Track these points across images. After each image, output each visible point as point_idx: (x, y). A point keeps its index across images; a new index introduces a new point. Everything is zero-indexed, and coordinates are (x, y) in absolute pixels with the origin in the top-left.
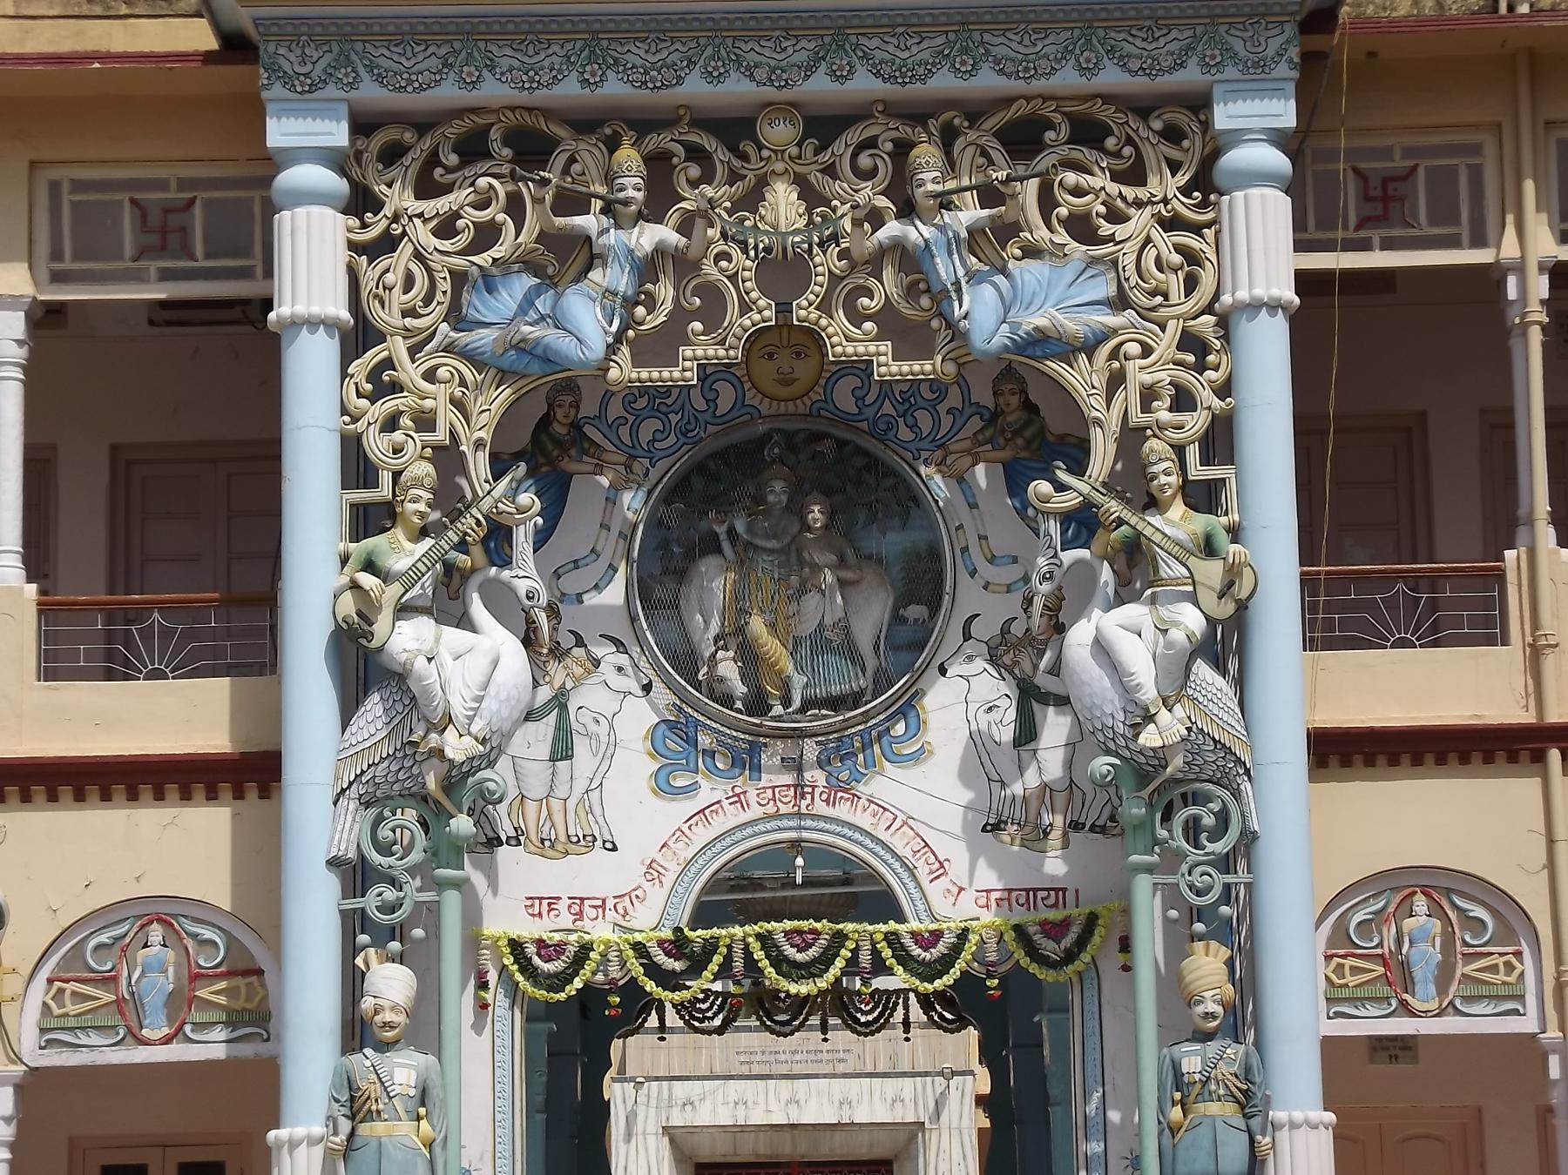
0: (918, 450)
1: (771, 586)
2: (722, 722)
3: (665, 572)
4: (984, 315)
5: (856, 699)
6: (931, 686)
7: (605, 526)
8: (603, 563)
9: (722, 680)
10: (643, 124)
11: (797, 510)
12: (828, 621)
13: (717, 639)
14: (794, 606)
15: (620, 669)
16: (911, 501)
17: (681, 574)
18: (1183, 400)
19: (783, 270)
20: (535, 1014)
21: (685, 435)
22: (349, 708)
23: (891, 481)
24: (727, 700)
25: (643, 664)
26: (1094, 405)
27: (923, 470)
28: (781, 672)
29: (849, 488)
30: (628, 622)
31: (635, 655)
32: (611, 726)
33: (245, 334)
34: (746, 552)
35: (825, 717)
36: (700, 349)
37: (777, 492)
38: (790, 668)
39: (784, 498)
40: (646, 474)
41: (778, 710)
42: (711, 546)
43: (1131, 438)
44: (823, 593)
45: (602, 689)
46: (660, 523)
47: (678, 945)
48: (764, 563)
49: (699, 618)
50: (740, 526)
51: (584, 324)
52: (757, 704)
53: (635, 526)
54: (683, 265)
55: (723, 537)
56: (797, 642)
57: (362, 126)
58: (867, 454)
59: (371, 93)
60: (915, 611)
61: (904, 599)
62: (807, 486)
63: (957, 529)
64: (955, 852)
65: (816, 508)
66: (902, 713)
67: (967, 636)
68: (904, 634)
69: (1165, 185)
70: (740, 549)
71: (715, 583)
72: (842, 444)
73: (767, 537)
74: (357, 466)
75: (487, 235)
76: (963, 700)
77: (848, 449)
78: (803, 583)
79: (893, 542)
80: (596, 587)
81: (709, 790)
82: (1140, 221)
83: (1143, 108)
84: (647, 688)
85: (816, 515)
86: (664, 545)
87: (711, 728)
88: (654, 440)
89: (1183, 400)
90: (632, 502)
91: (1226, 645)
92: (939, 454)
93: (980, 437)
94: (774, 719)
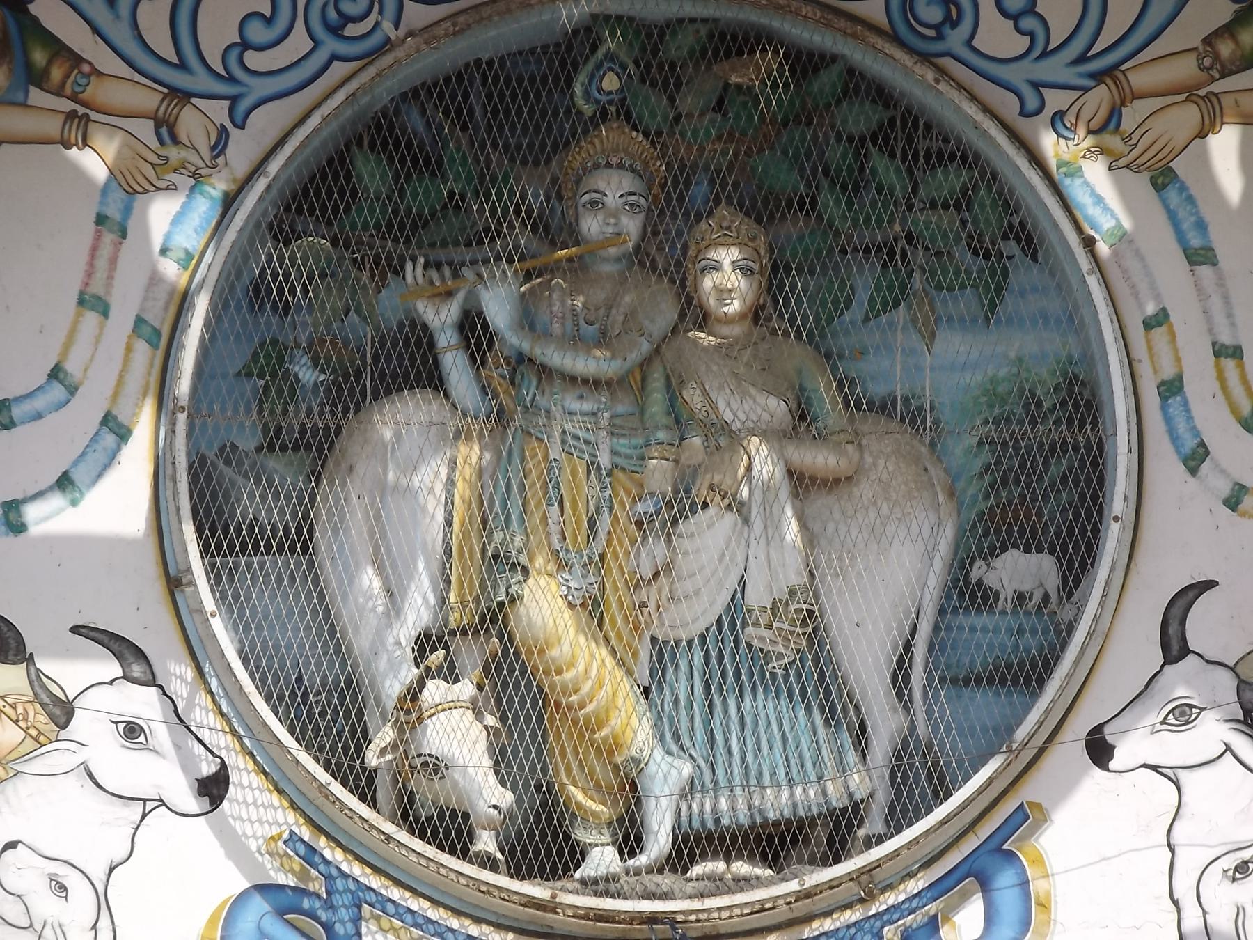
0: (1036, 86)
1: (587, 491)
3: (272, 443)
5: (836, 832)
6: (1067, 788)
7: (93, 302)
8: (85, 412)
9: (435, 767)
11: (666, 258)
12: (757, 596)
13: (424, 644)
14: (657, 550)
15: (132, 731)
16: (1006, 239)
17: (317, 449)
21: (335, 31)
22: (557, 913)
23: (949, 181)
24: (451, 831)
25: (203, 716)
27: (1050, 144)
28: (609, 749)
29: (829, 202)
30: (156, 589)
31: (179, 689)
32: (103, 902)
34: (515, 382)
35: (743, 883)
37: (611, 207)
38: (634, 727)
39: (632, 225)
40: (220, 145)
41: (603, 858)
42: (410, 365)
44: (740, 509)
45: (76, 786)
46: (258, 292)
48: (570, 414)
49: (370, 580)
50: (498, 306)
52: (543, 844)
53: (184, 302)
55: (446, 339)
56: (663, 653)
58: (882, 94)
60: (1019, 571)
61: (990, 532)
62: (700, 191)
63: (1149, 325)
65: (727, 256)
66: (977, 874)
67: (1174, 647)
68: (986, 636)
70: (496, 374)
71: (417, 476)
72: (806, 64)
73: (576, 341)
77: (827, 80)
78: (685, 481)
79: (955, 361)
80: (64, 482)
84: (213, 789)
85: (727, 277)
86: (268, 364)
87: (403, 913)
88: (245, 45)
90: (178, 229)
92: (1100, 97)
93: (1226, 49)
94: (592, 885)
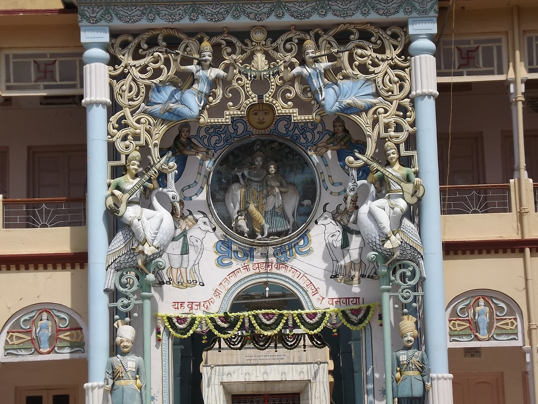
2: (241, 241)
4: (330, 99)
10: (211, 34)
18: (399, 128)
19: (260, 84)
20: (176, 343)
26: (368, 130)
33: (73, 107)
36: (232, 112)
37: (259, 161)
43: (381, 141)
47: (226, 318)
51: (192, 103)
54: (225, 82)
57: (114, 35)
59: (117, 23)
64: (321, 285)
69: (392, 53)
71: (238, 192)
74: (113, 153)
75: (157, 72)
76: (324, 232)
81: (236, 265)
82: (383, 66)
83: (384, 27)
89: (399, 128)
90: (209, 164)
91: (414, 213)
